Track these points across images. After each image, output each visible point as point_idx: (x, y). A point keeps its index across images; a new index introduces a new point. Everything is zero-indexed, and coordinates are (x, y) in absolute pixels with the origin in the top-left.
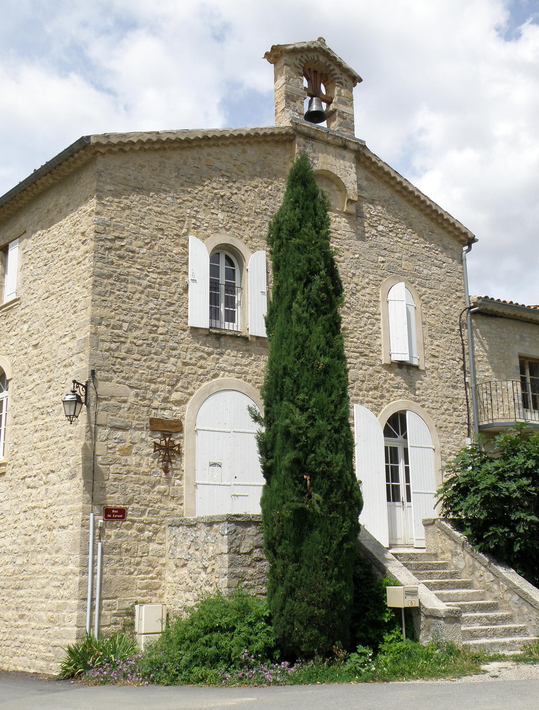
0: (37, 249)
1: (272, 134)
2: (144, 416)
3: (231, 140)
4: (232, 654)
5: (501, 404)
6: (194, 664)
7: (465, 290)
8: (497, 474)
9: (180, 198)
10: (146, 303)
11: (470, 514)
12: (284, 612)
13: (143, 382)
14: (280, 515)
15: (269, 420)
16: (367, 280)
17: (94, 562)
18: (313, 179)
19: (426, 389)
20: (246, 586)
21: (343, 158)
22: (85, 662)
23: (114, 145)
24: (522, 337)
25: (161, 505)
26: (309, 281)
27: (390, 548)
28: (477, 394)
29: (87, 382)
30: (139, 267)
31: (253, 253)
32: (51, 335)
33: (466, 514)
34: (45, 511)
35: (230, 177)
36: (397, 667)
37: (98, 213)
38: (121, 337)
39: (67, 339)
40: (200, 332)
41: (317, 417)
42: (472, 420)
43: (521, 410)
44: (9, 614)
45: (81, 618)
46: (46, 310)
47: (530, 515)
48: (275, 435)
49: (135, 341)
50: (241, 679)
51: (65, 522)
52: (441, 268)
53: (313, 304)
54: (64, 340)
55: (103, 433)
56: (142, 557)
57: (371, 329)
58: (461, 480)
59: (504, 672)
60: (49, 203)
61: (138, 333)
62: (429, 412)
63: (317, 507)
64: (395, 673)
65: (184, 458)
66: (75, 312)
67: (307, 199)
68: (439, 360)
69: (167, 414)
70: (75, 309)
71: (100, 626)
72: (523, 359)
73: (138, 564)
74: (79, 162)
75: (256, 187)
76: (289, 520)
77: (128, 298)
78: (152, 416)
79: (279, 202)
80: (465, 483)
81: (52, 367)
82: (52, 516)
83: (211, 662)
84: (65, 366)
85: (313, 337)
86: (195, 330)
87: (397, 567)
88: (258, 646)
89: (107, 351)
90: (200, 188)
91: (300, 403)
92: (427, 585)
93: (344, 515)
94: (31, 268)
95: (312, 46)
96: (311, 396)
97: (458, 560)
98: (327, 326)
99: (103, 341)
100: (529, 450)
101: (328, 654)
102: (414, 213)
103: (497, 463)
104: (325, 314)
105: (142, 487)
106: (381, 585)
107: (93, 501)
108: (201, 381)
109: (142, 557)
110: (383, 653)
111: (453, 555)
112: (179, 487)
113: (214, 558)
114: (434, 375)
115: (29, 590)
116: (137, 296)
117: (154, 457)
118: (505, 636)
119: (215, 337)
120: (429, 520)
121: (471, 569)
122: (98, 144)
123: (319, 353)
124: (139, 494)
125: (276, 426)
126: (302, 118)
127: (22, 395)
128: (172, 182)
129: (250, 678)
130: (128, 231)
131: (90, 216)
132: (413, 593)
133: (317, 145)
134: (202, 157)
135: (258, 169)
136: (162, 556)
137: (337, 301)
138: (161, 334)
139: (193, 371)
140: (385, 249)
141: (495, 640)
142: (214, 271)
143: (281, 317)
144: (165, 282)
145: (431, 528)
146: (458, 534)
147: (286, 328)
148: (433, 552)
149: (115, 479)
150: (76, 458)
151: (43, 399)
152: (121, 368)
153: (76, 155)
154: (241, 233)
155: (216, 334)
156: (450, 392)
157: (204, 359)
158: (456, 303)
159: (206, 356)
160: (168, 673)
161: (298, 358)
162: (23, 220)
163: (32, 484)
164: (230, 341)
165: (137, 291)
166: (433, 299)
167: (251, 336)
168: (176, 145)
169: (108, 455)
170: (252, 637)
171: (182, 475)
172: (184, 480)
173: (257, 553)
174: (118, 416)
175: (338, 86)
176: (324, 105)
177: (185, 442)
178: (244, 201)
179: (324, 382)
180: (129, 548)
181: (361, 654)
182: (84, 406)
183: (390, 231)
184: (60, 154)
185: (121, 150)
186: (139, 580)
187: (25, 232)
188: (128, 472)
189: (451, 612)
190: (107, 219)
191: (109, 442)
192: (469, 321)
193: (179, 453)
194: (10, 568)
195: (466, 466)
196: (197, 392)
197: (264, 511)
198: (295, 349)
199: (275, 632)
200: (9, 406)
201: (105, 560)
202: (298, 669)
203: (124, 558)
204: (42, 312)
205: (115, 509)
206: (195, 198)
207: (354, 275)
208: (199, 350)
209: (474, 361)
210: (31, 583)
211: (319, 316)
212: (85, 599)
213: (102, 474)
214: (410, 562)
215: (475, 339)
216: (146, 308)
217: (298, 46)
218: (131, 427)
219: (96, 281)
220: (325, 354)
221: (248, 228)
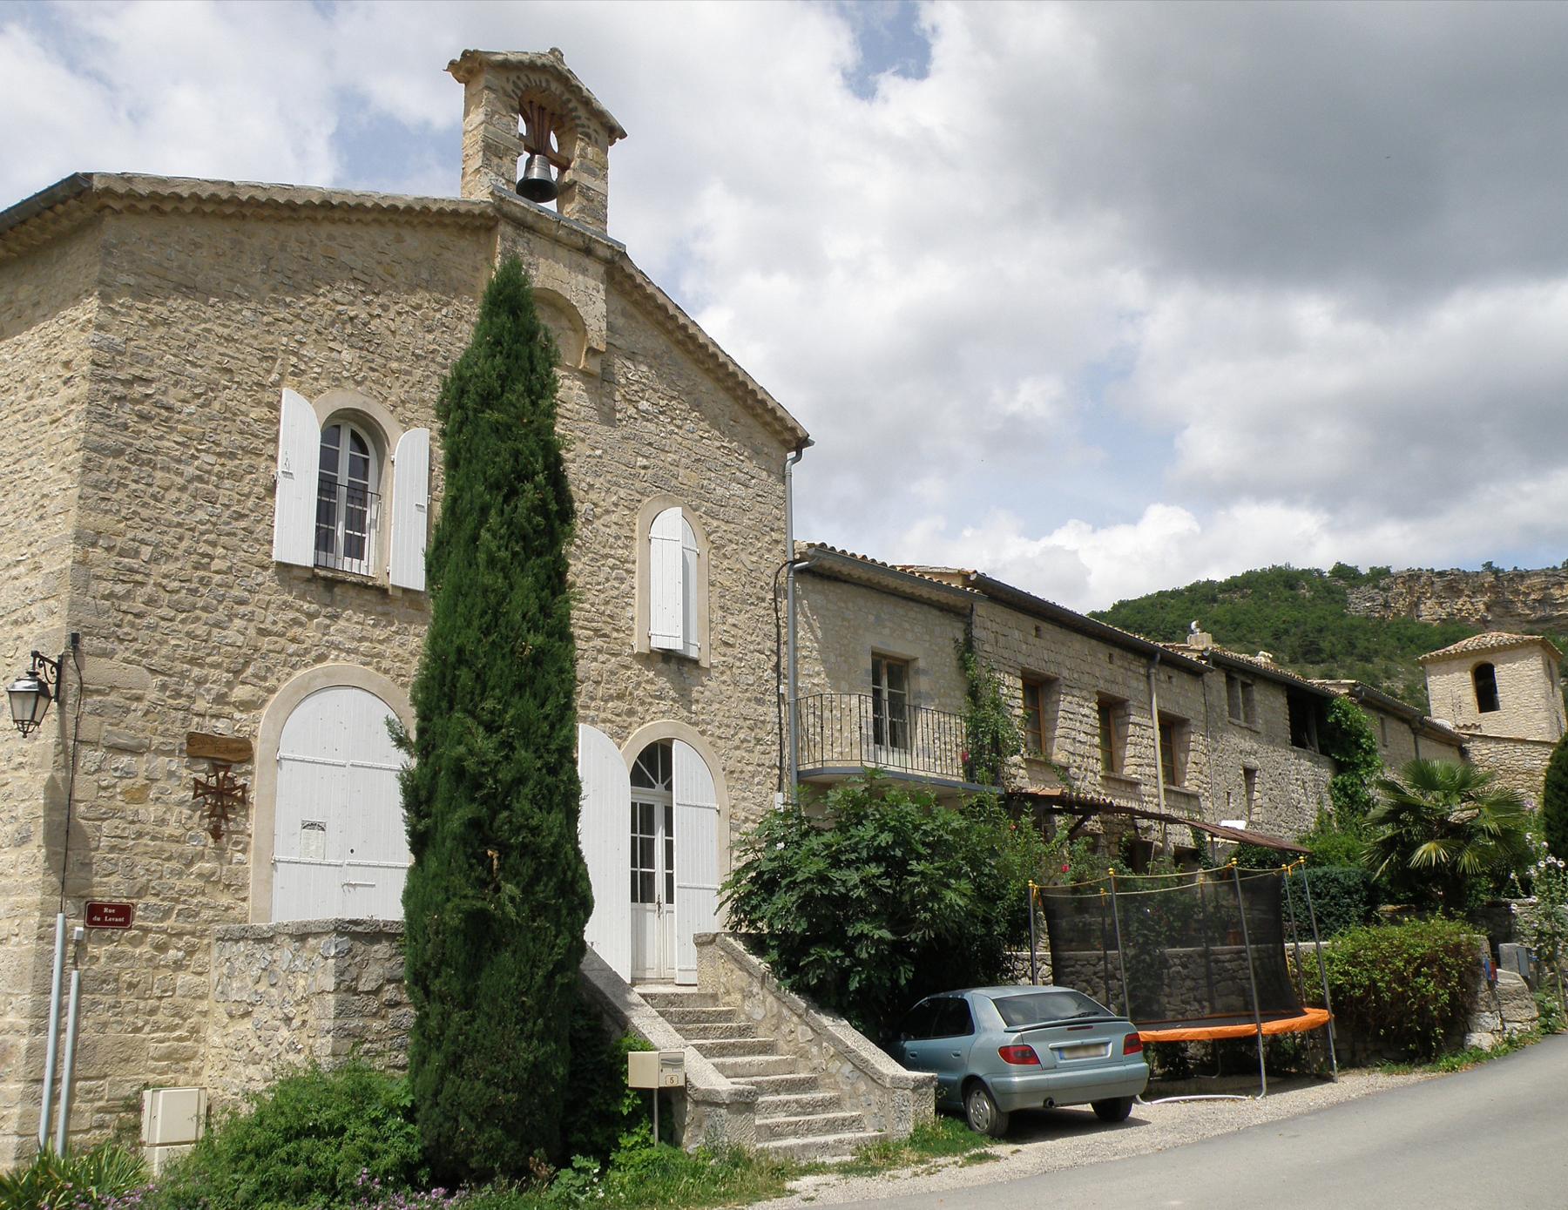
1: (455, 213)
3: (374, 215)
4: (339, 1178)
5: (837, 734)
6: (262, 1197)
7: (787, 530)
10: (191, 511)
12: (440, 1099)
13: (177, 663)
14: (441, 922)
15: (425, 746)
16: (614, 498)
17: (61, 1008)
18: (530, 304)
20: (367, 1052)
21: (584, 271)
23: (141, 198)
24: (878, 617)
25: (204, 900)
26: (513, 493)
27: (633, 984)
28: (798, 716)
29: (61, 657)
30: (180, 439)
31: (405, 430)
33: (770, 925)
35: (369, 286)
36: (643, 1191)
37: (100, 327)
38: (137, 572)
39: (22, 569)
40: (296, 572)
41: (517, 744)
42: (786, 761)
43: (871, 748)
45: (27, 1119)
47: (880, 928)
48: (435, 774)
53: (517, 534)
54: (14, 572)
55: (90, 757)
58: (766, 866)
61: (171, 567)
63: (510, 909)
65: (253, 812)
66: (42, 517)
67: (517, 338)
68: (736, 651)
69: (221, 726)
70: (41, 511)
71: (67, 1133)
73: (153, 1012)
74: (65, 223)
75: (419, 307)
76: (456, 932)
77: (154, 497)
78: (192, 729)
79: (460, 340)
80: (773, 871)
83: (296, 1193)
84: (16, 622)
85: (517, 597)
86: (284, 567)
89: (104, 597)
90: (310, 299)
91: (486, 717)
92: (699, 1048)
93: (558, 924)
95: (539, 62)
96: (507, 705)
98: (543, 577)
99: (98, 578)
100: (883, 816)
101: (520, 1173)
102: (706, 385)
103: (828, 837)
104: (539, 555)
105: (167, 865)
106: (619, 1048)
107: (64, 889)
108: (293, 667)
110: (618, 1168)
117: (193, 809)
118: (828, 1132)
119: (324, 585)
121: (774, 1021)
122: (108, 192)
123: (525, 626)
124: (160, 878)
125: (439, 757)
126: (513, 189)
128: (255, 281)
131: (82, 330)
132: (676, 1063)
135: (425, 275)
136: (201, 998)
138: (217, 572)
139: (278, 647)
140: (650, 444)
141: (810, 1139)
142: (328, 459)
143: (456, 556)
145: (709, 950)
146: (754, 959)
148: (710, 991)
149: (112, 849)
150: (31, 804)
152: (134, 634)
153: (60, 208)
155: (325, 579)
156: (751, 710)
157: (301, 624)
158: (769, 551)
159: (303, 619)
161: (487, 633)
164: (352, 593)
167: (394, 587)
169: (100, 802)
170: (379, 1146)
171: (248, 843)
172: (251, 855)
173: (390, 992)
176: (554, 170)
178: (393, 332)
179: (532, 679)
180: (135, 980)
181: (579, 1170)
182: (54, 704)
184: (23, 203)
185: (155, 208)
186: (154, 1043)
188: (140, 835)
189: (739, 1093)
190: (118, 340)
191: (102, 775)
193: (244, 802)
195: (773, 842)
196: (284, 686)
197: (408, 915)
201: (85, 1003)
202: (462, 1200)
203: (123, 1000)
205: (110, 907)
206: (298, 316)
207: (591, 486)
208: (291, 607)
209: (795, 657)
211: (528, 559)
212: (40, 1081)
213: (86, 839)
214: (667, 1006)
216: (191, 520)
217: (511, 57)
218: (148, 749)
219: (89, 460)
220: (535, 628)
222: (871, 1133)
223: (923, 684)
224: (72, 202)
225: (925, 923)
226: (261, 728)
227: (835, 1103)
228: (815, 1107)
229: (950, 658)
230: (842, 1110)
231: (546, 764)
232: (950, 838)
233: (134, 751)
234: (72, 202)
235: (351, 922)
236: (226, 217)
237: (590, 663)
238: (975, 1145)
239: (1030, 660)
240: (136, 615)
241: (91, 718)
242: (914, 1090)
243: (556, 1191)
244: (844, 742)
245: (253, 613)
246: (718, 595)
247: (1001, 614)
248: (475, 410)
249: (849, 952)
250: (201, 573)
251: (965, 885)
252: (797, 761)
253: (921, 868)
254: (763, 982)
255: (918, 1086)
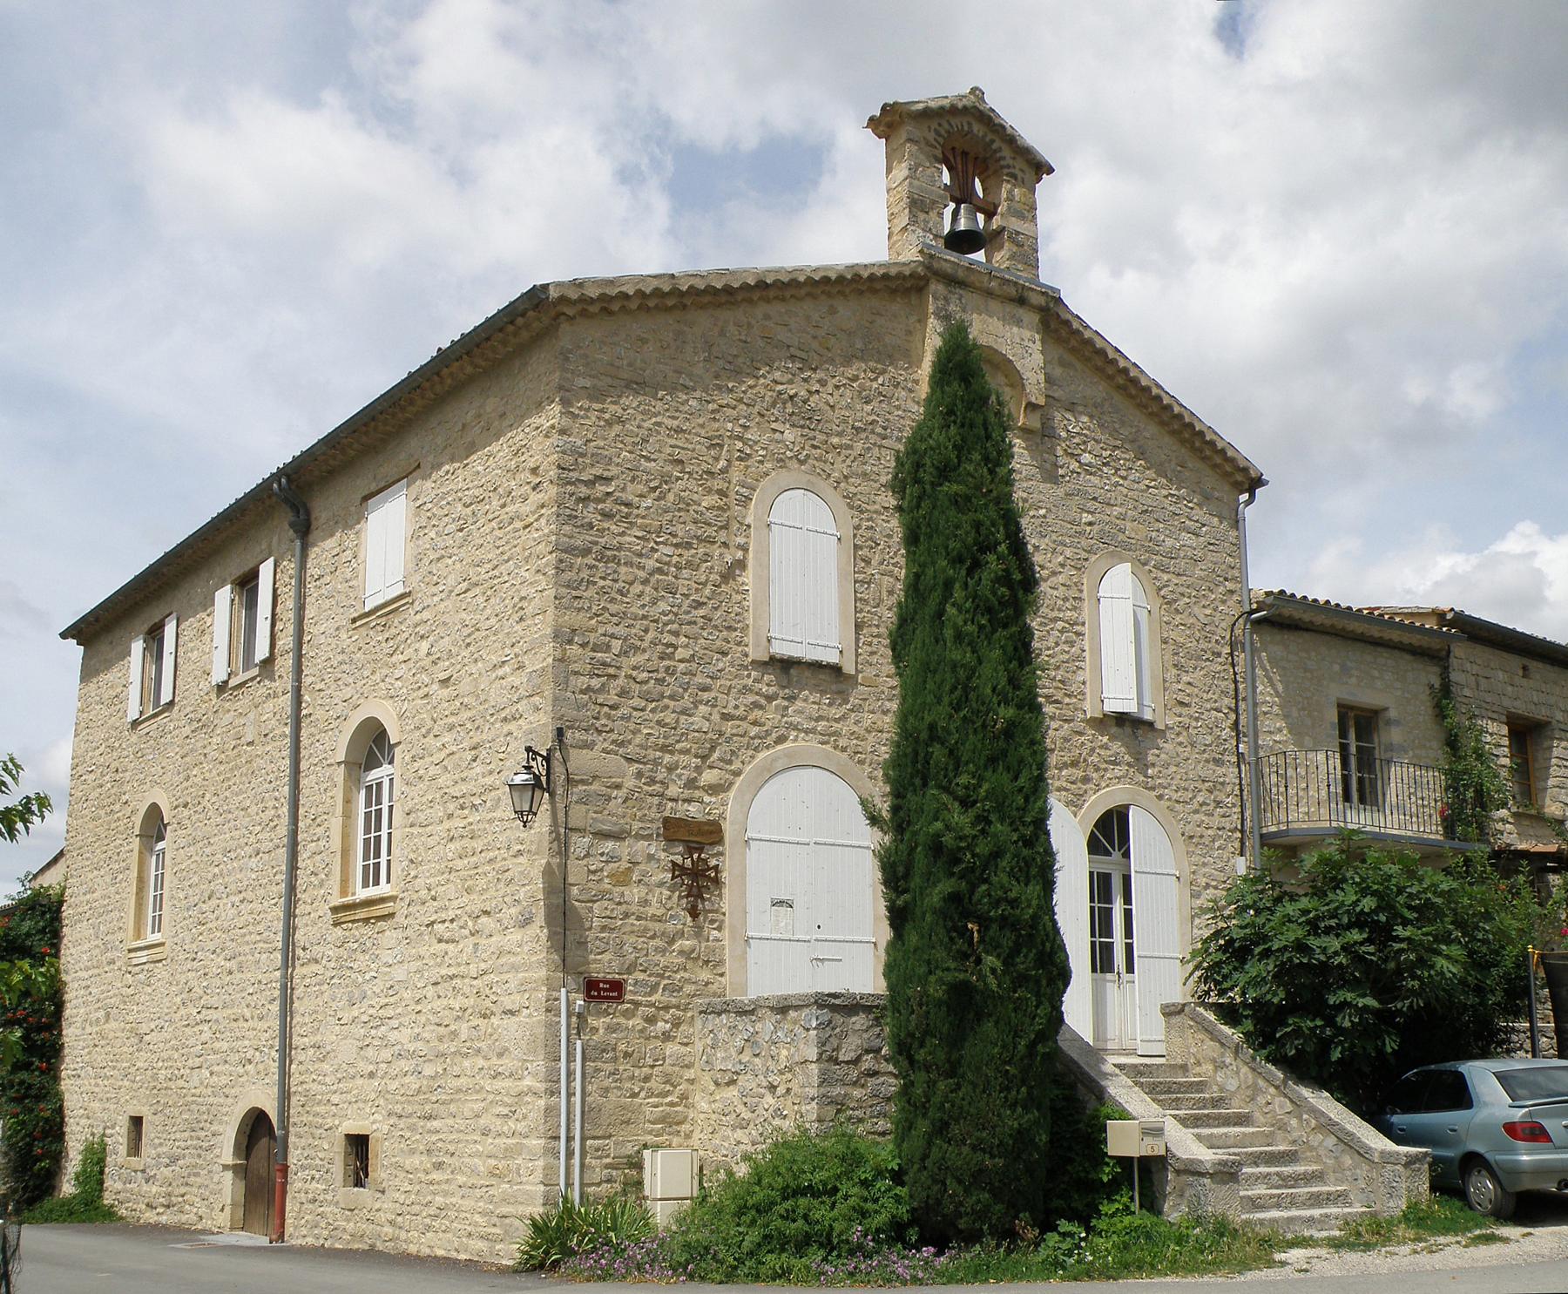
1: (886, 277)
2: (653, 814)
7: (1242, 578)
8: (1308, 922)
11: (1251, 995)
14: (925, 993)
16: (1061, 559)
19: (1166, 766)
21: (1019, 323)
22: (563, 1244)
23: (592, 301)
25: (686, 975)
26: (976, 565)
28: (1259, 775)
30: (640, 534)
33: (1243, 994)
37: (563, 432)
39: (507, 669)
41: (993, 817)
42: (1248, 823)
44: (414, 1161)
45: (550, 1170)
46: (464, 615)
47: (1364, 996)
48: (912, 850)
50: (851, 1274)
51: (513, 1002)
52: (1197, 535)
54: (500, 672)
55: (580, 843)
56: (653, 1067)
59: (1318, 1265)
60: (465, 410)
62: (1170, 809)
63: (992, 980)
64: (1126, 1266)
65: (726, 891)
66: (521, 619)
68: (1192, 711)
69: (693, 810)
71: (582, 1185)
72: (1344, 710)
73: (647, 1079)
74: (525, 335)
75: (855, 378)
76: (939, 1003)
80: (1244, 939)
82: (488, 991)
84: (505, 719)
85: (986, 670)
88: (881, 1219)
89: (582, 692)
91: (961, 792)
93: (1038, 994)
94: (433, 534)
95: (960, 105)
96: (981, 779)
98: (1010, 649)
99: (576, 673)
101: (1008, 1235)
102: (1150, 430)
104: (1005, 626)
106: (1097, 1117)
107: (565, 965)
109: (653, 1067)
110: (1100, 1234)
111: (1217, 1068)
114: (1181, 739)
115: (450, 1121)
117: (672, 889)
118: (1312, 1206)
121: (1249, 1092)
122: (563, 299)
125: (915, 833)
127: (421, 772)
128: (699, 370)
129: (868, 1273)
131: (547, 436)
132: (1156, 1132)
133: (968, 296)
137: (1027, 602)
138: (681, 661)
140: (1095, 499)
141: (1294, 1213)
143: (922, 633)
145: (1176, 1020)
149: (603, 928)
150: (533, 888)
151: (463, 780)
153: (520, 321)
154: (827, 468)
156: (1210, 771)
157: (761, 707)
158: (1224, 602)
159: (763, 702)
160: (722, 1262)
161: (957, 708)
162: (415, 445)
163: (447, 936)
164: (807, 673)
168: (706, 299)
169: (590, 885)
170: (869, 1206)
171: (722, 921)
172: (726, 932)
173: (868, 1062)
176: (981, 217)
177: (728, 862)
179: (1004, 753)
181: (1064, 1235)
185: (604, 309)
186: (650, 1108)
188: (626, 915)
190: (579, 443)
191: (591, 860)
193: (717, 882)
194: (413, 1082)
196: (748, 768)
197: (891, 987)
198: (952, 692)
199: (911, 1197)
200: (396, 793)
201: (589, 1070)
206: (740, 400)
209: (1255, 713)
211: (994, 631)
212: (557, 1138)
215: (1258, 671)
216: (654, 612)
217: (932, 104)
219: (561, 561)
221: (840, 459)
222: (1358, 1209)
223: (1395, 735)
224: (531, 313)
225: (1412, 992)
226: (729, 810)
228: (1297, 1180)
229: (1422, 708)
230: (1325, 1184)
231: (1022, 837)
232: (1439, 901)
233: (617, 836)
234: (531, 313)
235: (829, 995)
236: (668, 309)
238: (1478, 1226)
239: (1517, 703)
240: (611, 707)
241: (578, 807)
242: (1406, 1165)
243: (1044, 1252)
244: (1310, 801)
245: (716, 698)
246: (1172, 654)
247: (1482, 654)
248: (932, 484)
249: (1330, 1022)
250: (667, 663)
251: (1455, 951)
253: (1407, 934)
254: (1236, 1053)
255: (1411, 1162)
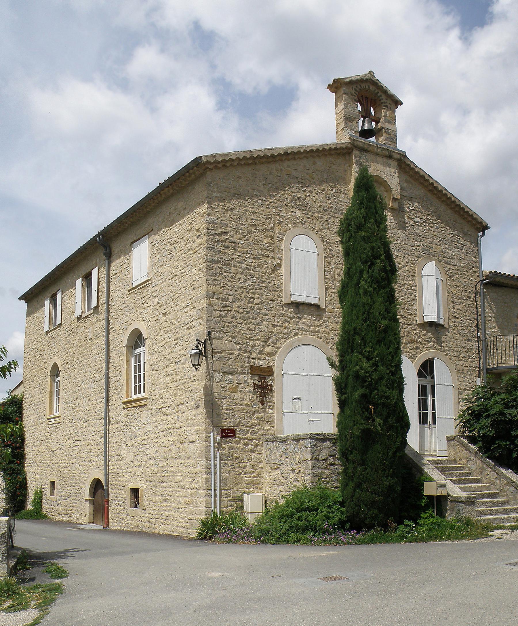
0: (162, 242)
1: (336, 149)
2: (246, 364)
7: (480, 266)
8: (504, 404)
9: (268, 201)
12: (354, 499)
13: (244, 340)
16: (407, 260)
17: (215, 465)
19: (449, 342)
20: (323, 482)
21: (389, 165)
23: (219, 162)
25: (260, 427)
26: (372, 264)
28: (486, 345)
32: (176, 306)
33: (478, 432)
34: (178, 431)
37: (208, 215)
39: (188, 308)
41: (379, 364)
42: (482, 365)
45: (208, 502)
46: (171, 288)
48: (347, 378)
49: (238, 309)
50: (324, 541)
52: (462, 250)
54: (186, 310)
55: (218, 376)
56: (247, 462)
57: (410, 298)
60: (170, 207)
61: (239, 304)
62: (450, 359)
63: (379, 428)
64: (431, 537)
65: (275, 394)
69: (262, 362)
71: (220, 507)
73: (245, 467)
74: (193, 176)
75: (324, 190)
76: (358, 437)
80: (479, 410)
81: (178, 329)
82: (183, 434)
85: (376, 306)
87: (431, 469)
89: (218, 317)
94: (158, 256)
95: (365, 78)
96: (374, 349)
97: (472, 464)
99: (215, 310)
101: (385, 526)
102: (442, 207)
104: (384, 288)
107: (212, 424)
109: (247, 462)
112: (272, 415)
113: (300, 463)
114: (455, 331)
115: (170, 484)
116: (239, 276)
118: (504, 514)
120: (451, 436)
121: (480, 470)
122: (208, 162)
125: (349, 371)
126: (358, 135)
128: (262, 188)
130: (230, 227)
131: (202, 216)
132: (443, 486)
134: (283, 168)
135: (325, 176)
136: (261, 462)
138: (256, 304)
139: (280, 331)
140: (420, 236)
143: (351, 292)
144: (258, 265)
145: (452, 442)
147: (355, 299)
149: (227, 409)
151: (172, 352)
153: (191, 171)
156: (467, 344)
157: (288, 322)
158: (472, 276)
159: (289, 320)
160: (274, 536)
161: (365, 321)
162: (151, 221)
165: (238, 272)
166: (456, 274)
170: (331, 515)
171: (274, 406)
173: (331, 460)
174: (228, 364)
175: (384, 109)
176: (373, 123)
177: (275, 383)
179: (384, 339)
181: (407, 526)
182: (204, 358)
183: (424, 222)
185: (224, 166)
186: (246, 478)
187: (153, 230)
188: (236, 404)
190: (215, 219)
192: (482, 290)
193: (271, 391)
197: (339, 431)
198: (363, 315)
199: (347, 511)
200: (146, 358)
204: (168, 289)
205: (228, 430)
206: (278, 200)
209: (485, 321)
210: (170, 478)
211: (380, 290)
216: (245, 285)
217: (353, 79)
218: (237, 372)
219: (209, 266)
220: (384, 318)
226: (276, 362)
227: (507, 503)
230: (510, 505)
233: (232, 373)
234: (195, 168)
235: (316, 434)
236: (249, 165)
237: (404, 330)
243: (398, 532)
246: (451, 296)
249: (513, 442)
252: (486, 364)
